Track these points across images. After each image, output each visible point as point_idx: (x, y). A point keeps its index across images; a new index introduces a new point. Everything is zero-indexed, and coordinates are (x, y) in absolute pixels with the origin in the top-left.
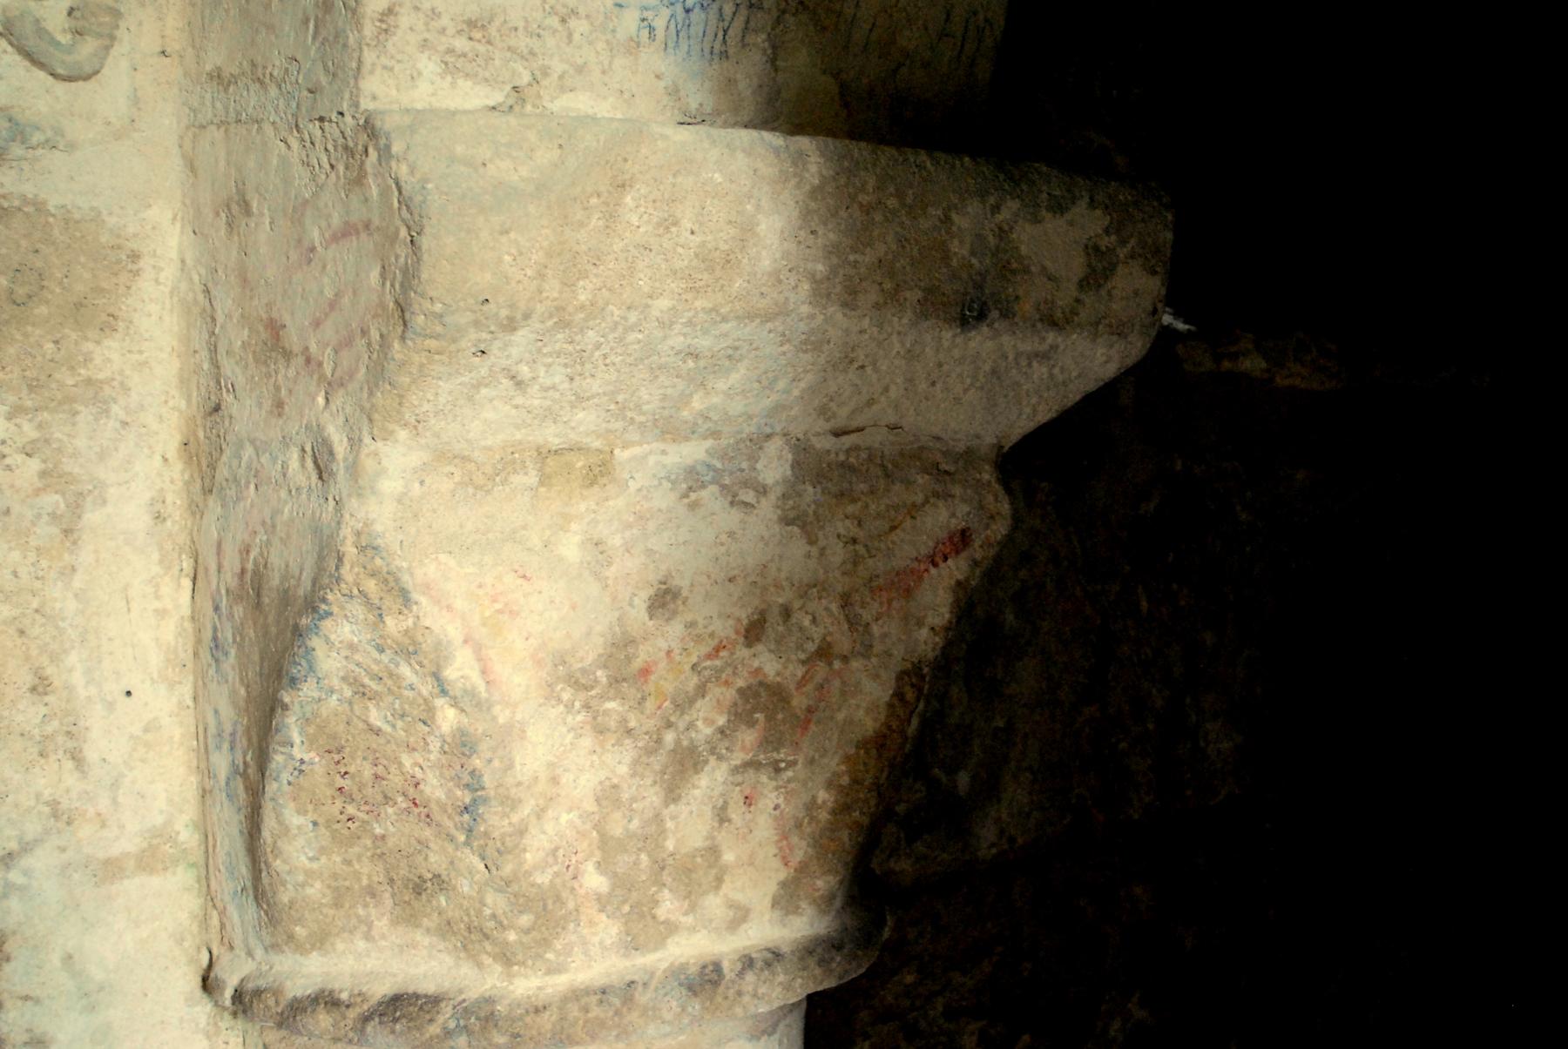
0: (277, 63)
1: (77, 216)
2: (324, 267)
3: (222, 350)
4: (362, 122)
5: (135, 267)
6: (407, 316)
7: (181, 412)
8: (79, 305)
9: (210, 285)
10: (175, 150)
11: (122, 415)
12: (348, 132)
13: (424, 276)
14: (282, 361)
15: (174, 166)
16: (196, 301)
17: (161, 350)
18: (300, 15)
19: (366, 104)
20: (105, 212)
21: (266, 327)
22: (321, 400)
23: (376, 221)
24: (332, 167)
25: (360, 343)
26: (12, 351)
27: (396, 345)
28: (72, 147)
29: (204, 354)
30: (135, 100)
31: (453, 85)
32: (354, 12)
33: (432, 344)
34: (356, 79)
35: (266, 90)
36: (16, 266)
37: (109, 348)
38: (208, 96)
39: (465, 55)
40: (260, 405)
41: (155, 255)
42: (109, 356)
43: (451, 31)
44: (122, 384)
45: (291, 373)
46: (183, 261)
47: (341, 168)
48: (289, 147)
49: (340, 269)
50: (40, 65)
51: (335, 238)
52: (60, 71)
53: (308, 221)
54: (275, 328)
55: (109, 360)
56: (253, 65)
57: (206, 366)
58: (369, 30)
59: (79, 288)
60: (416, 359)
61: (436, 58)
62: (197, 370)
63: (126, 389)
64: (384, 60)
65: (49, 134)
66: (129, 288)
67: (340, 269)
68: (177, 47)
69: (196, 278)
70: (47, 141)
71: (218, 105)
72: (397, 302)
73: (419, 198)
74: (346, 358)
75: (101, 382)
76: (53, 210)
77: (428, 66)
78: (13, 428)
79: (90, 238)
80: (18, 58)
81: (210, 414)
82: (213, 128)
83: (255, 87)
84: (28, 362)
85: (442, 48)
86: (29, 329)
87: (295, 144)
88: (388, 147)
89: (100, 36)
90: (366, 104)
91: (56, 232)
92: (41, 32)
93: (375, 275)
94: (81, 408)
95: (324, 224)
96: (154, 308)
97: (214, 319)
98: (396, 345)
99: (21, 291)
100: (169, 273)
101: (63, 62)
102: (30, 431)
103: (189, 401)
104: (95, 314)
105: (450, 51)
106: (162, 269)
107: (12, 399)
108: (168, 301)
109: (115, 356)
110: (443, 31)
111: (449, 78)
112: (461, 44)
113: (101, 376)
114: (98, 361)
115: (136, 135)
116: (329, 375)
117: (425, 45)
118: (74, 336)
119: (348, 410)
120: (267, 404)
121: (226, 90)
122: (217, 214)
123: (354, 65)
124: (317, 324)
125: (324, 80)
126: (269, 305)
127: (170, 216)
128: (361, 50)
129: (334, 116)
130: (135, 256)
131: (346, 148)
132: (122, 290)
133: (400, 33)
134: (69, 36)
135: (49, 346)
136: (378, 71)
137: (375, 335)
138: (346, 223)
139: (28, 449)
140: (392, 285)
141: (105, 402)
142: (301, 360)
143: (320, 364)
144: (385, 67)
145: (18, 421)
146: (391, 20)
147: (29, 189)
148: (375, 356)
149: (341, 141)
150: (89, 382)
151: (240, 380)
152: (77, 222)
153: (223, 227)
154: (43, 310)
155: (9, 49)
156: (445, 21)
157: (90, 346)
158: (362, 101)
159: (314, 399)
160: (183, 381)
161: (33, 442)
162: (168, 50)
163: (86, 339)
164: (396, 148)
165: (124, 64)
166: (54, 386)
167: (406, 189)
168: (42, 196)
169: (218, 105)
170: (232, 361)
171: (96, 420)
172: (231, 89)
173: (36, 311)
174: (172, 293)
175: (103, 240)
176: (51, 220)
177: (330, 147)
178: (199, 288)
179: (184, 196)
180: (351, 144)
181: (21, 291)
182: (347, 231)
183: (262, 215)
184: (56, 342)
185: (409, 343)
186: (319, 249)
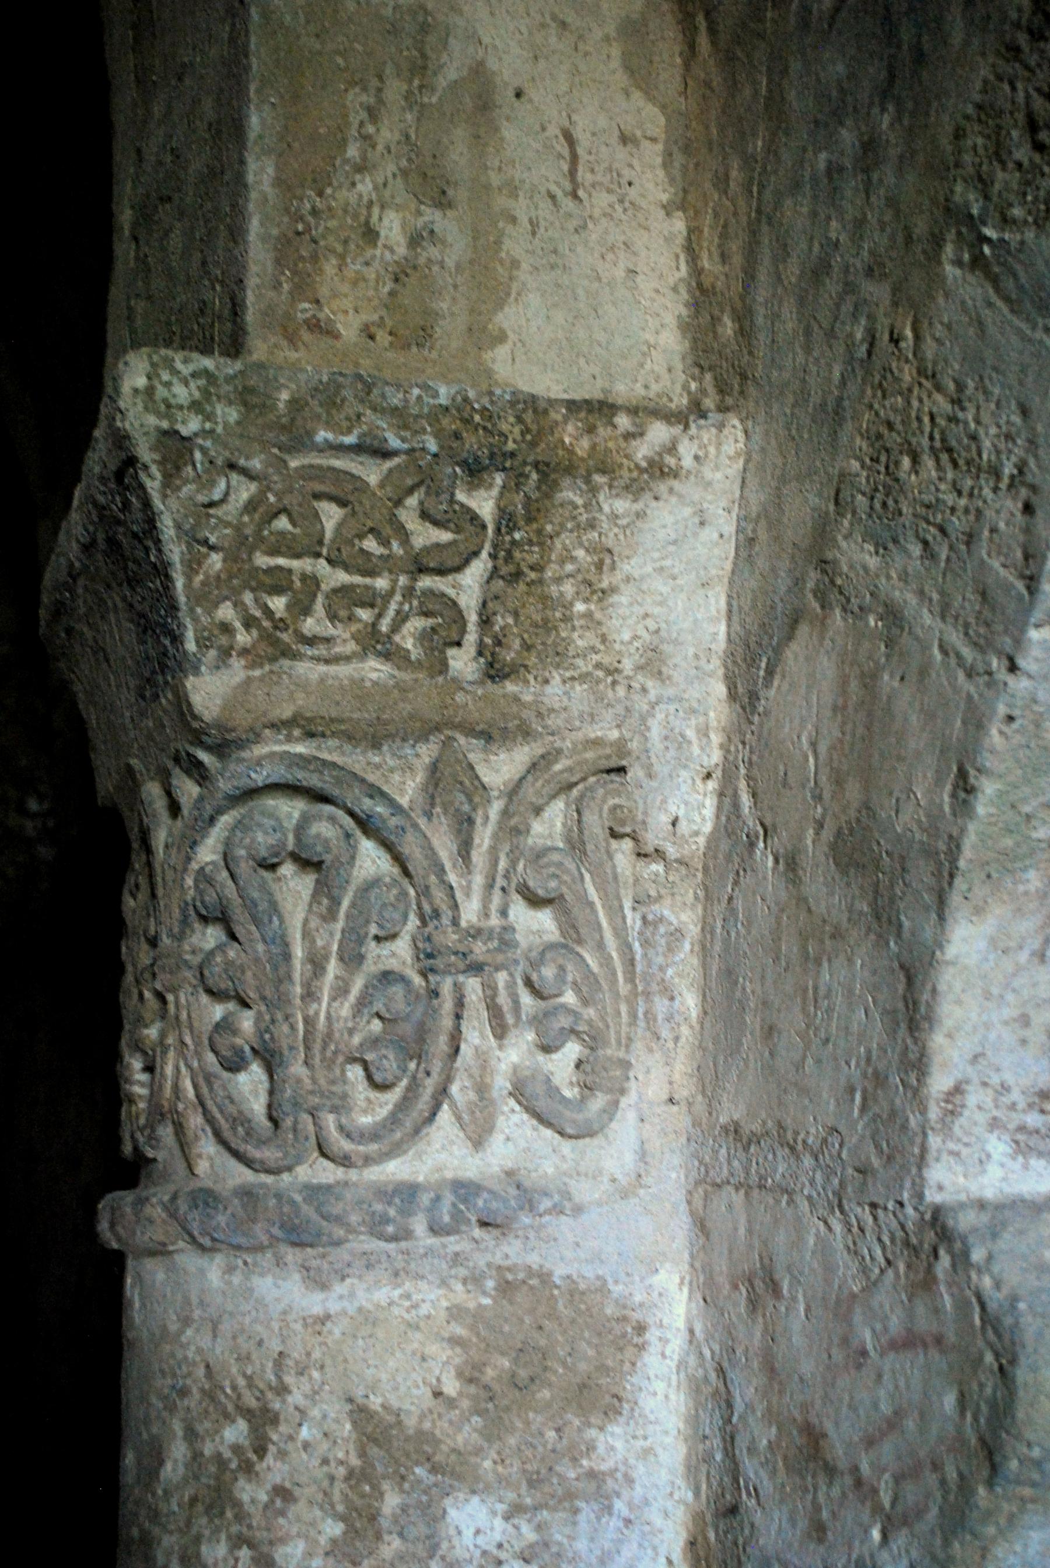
0: (813, 1130)
1: (582, 1286)
2: (880, 1376)
3: (742, 1443)
4: (928, 1217)
5: (640, 1340)
6: (997, 1459)
7: (686, 1504)
8: (583, 1386)
9: (725, 1364)
10: (683, 1207)
11: (625, 1512)
12: (910, 1226)
13: (1020, 1415)
14: (822, 1480)
15: (681, 1227)
16: (706, 1379)
17: (666, 1433)
18: (843, 1081)
19: (932, 1196)
20: (610, 1280)
21: (801, 1431)
22: (876, 1534)
23: (951, 1337)
24: (889, 1262)
25: (931, 1479)
26: (512, 1441)
27: (982, 1491)
28: (578, 1210)
29: (717, 1442)
30: (643, 1155)
31: (1026, 1167)
32: (916, 1092)
33: (1027, 1491)
34: (920, 1168)
35: (798, 1158)
36: (519, 1346)
37: (612, 1434)
38: (723, 1151)
39: (1037, 1132)
40: (793, 1522)
41: (661, 1326)
42: (613, 1444)
43: (1021, 1105)
44: (626, 1475)
45: (836, 1492)
46: (691, 1331)
47: (902, 1267)
48: (830, 1229)
49: (902, 1384)
50: (549, 1124)
51: (895, 1346)
52: (570, 1131)
53: (858, 1318)
54: (813, 1438)
55: (612, 1448)
56: (781, 1126)
57: (719, 1457)
58: (934, 1113)
59: (583, 1366)
60: (1005, 1506)
61: (1006, 1137)
62: (708, 1458)
63: (630, 1481)
64: (951, 1145)
65: (557, 1198)
66: (633, 1364)
67: (902, 1384)
68: (685, 1093)
69: (707, 1353)
70: (555, 1206)
71: (736, 1163)
72: (982, 1440)
73: (1008, 1321)
74: (911, 1493)
75: (603, 1473)
76: (558, 1282)
77: (998, 1146)
78: (510, 1529)
79: (595, 1310)
80: (525, 1116)
81: (725, 1515)
82: (730, 1188)
83: (782, 1152)
84: (529, 1453)
85: (1011, 1126)
86: (531, 1415)
87: (838, 1227)
88: (966, 1254)
89: (610, 1091)
90: (932, 1196)
91: (560, 1306)
92: (553, 1091)
93: (950, 1401)
94: (582, 1505)
95: (878, 1327)
96: (660, 1386)
97: (730, 1405)
98: (982, 1491)
99: (523, 1373)
100: (677, 1345)
101: (574, 1122)
102: (529, 1534)
103: (697, 1493)
104: (600, 1397)
105: (1022, 1128)
106: (667, 1341)
107: (511, 1496)
108: (674, 1377)
109: (619, 1445)
110: (1013, 1107)
111: (1020, 1159)
112: (1033, 1119)
113: (604, 1467)
114: (601, 1449)
115: (642, 1192)
116: (887, 1505)
117: (994, 1124)
118: (577, 1422)
119: (914, 1554)
120: (803, 1524)
121: (746, 1149)
122: (736, 1287)
123: (916, 1151)
124: (870, 1442)
125: (876, 1162)
126: (805, 1407)
127: (677, 1280)
128: (925, 1134)
129: (890, 1205)
130: (641, 1329)
131: (907, 1243)
132: (627, 1366)
133: (966, 1113)
134: (576, 1090)
135: (551, 1434)
136: (945, 1156)
137: (951, 1474)
138: (909, 1331)
139: (526, 1555)
140: (976, 1419)
141: (608, 1498)
142: (848, 1480)
143: (875, 1491)
144: (951, 1153)
145: (516, 1521)
146: (957, 1099)
147: (534, 1260)
148: (952, 1497)
149: (900, 1234)
150: (592, 1474)
151: (767, 1486)
152: (583, 1293)
153: (743, 1303)
154: (546, 1394)
155: (517, 1108)
156: (1016, 1096)
157: (593, 1433)
158: (927, 1193)
159: (867, 1531)
160: (691, 1470)
161: (531, 1546)
162: (676, 1097)
163: (589, 1425)
164: (977, 1255)
165: (631, 1116)
166: (555, 1481)
167: (992, 1306)
168: (548, 1265)
169: (736, 1163)
170: (756, 1461)
171: (598, 1519)
172: (753, 1149)
173: (539, 1396)
174: (678, 1367)
175: (609, 1311)
176: (556, 1292)
177: (886, 1239)
178: (710, 1365)
179: (692, 1256)
180: (914, 1240)
181: (523, 1373)
182: (908, 1342)
183: (794, 1299)
184: (558, 1430)
185: (999, 1490)
186: (872, 1353)
